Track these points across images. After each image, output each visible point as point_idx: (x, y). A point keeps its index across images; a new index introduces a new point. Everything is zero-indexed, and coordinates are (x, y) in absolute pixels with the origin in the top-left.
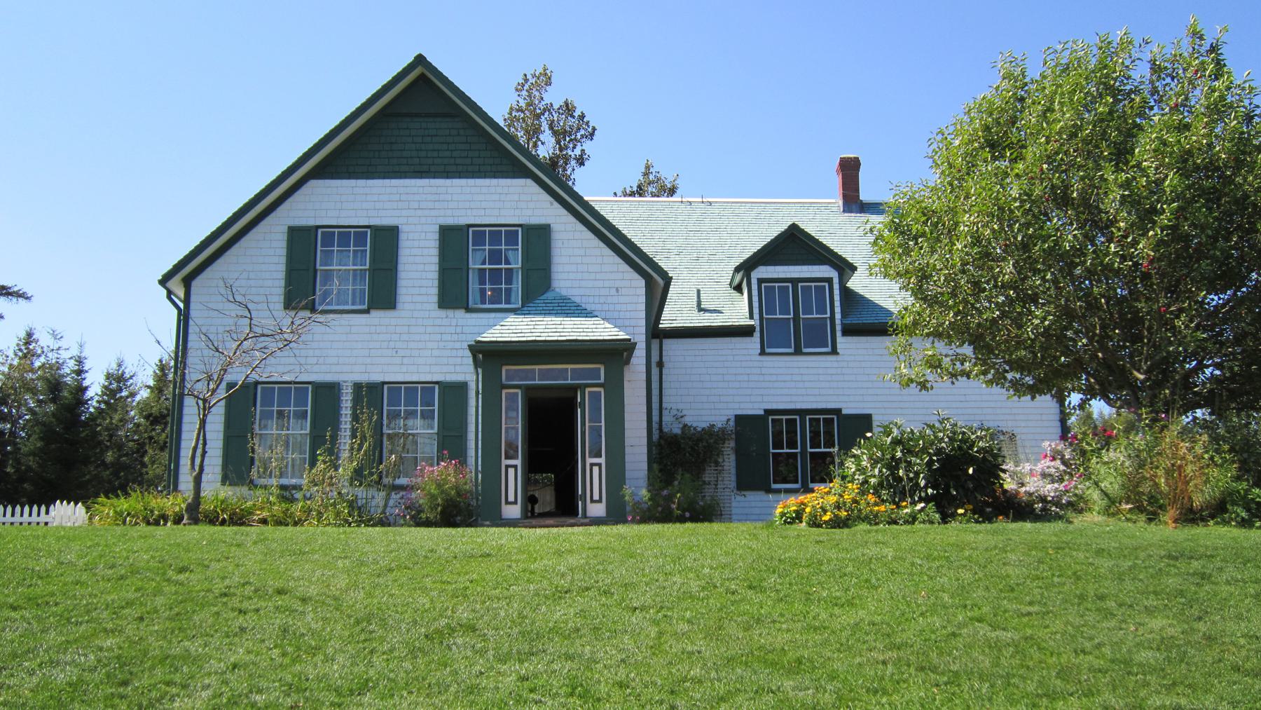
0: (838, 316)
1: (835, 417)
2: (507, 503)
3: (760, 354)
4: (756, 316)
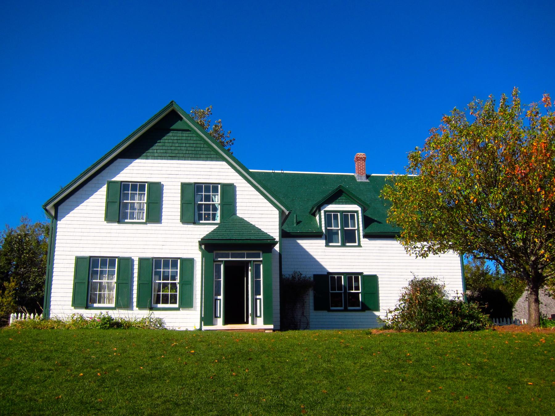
4: (323, 229)
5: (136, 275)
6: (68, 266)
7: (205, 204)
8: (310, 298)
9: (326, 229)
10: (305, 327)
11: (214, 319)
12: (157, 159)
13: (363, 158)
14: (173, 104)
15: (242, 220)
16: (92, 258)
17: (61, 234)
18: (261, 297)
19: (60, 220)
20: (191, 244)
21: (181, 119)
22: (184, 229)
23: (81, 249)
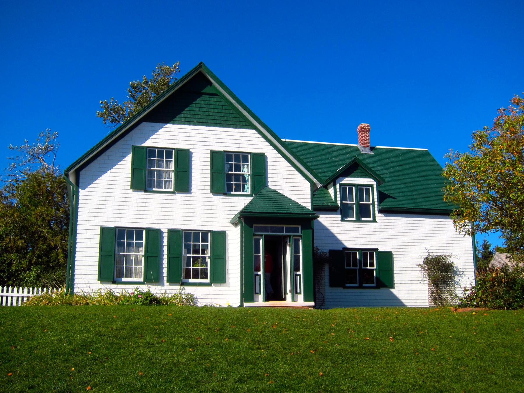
4: (339, 202)
5: (165, 248)
6: (92, 237)
7: (235, 174)
9: (341, 203)
10: (321, 304)
11: (255, 296)
12: (185, 124)
13: (368, 128)
14: (201, 66)
15: (275, 192)
16: (117, 229)
17: (84, 201)
18: (301, 273)
19: (84, 188)
20: (221, 216)
21: (210, 84)
22: (215, 200)
23: (106, 219)
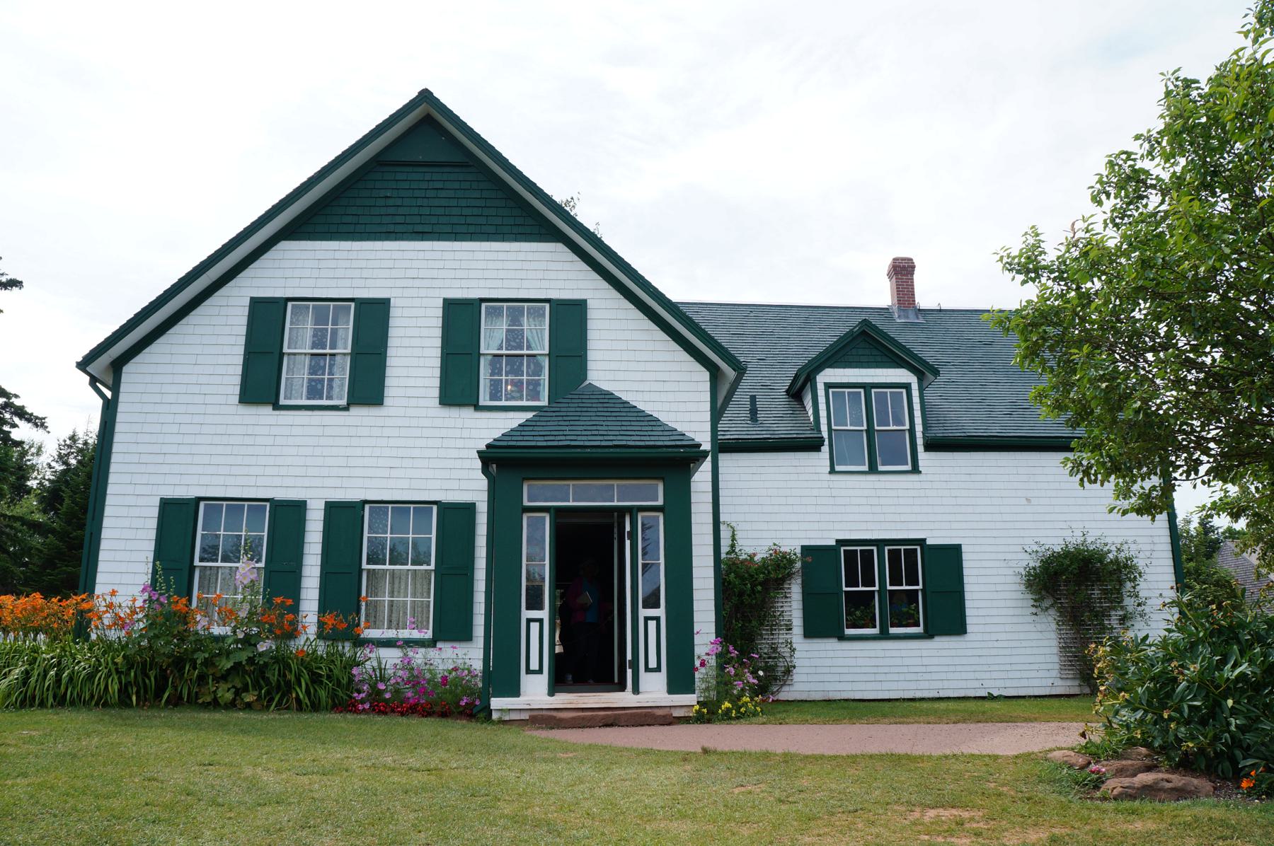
0: (919, 428)
1: (918, 548)
2: (529, 671)
3: (830, 473)
4: (824, 428)
8: (793, 605)
